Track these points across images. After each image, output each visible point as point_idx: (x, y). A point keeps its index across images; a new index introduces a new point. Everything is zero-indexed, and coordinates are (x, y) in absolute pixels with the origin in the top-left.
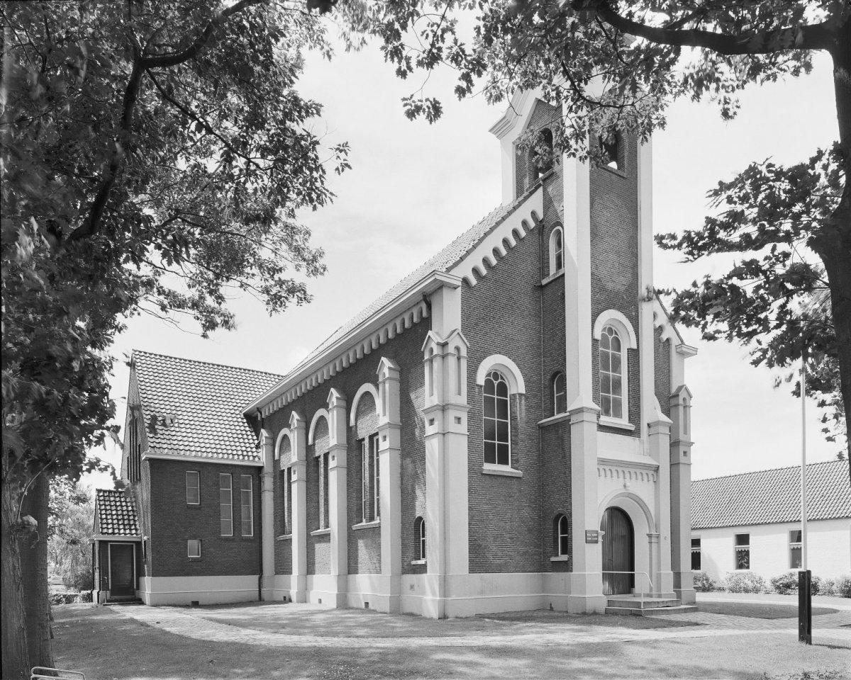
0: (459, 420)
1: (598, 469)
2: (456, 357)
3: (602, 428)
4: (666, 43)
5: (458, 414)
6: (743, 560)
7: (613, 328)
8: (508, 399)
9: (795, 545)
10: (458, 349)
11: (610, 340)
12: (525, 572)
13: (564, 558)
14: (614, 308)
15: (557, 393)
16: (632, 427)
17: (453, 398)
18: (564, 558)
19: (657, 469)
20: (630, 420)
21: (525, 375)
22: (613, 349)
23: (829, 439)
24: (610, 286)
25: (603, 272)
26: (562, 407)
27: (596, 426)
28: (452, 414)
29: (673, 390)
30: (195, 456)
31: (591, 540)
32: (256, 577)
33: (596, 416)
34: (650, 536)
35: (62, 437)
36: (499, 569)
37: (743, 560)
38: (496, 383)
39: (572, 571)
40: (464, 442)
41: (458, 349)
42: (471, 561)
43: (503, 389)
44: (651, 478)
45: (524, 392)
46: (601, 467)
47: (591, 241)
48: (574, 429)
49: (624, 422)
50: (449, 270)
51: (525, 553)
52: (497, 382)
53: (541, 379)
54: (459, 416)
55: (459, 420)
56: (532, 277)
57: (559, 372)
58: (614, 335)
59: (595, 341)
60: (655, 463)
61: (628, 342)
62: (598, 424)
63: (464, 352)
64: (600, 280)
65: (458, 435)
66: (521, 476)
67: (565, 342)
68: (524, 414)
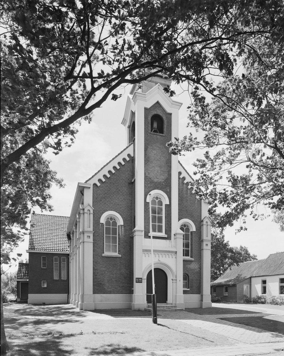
5: (89, 235)
6: (264, 290)
7: (159, 197)
8: (117, 227)
9: (264, 285)
12: (123, 294)
14: (157, 189)
16: (166, 236)
17: (86, 229)
19: (176, 253)
20: (166, 233)
22: (159, 205)
25: (152, 175)
28: (86, 235)
29: (202, 218)
30: (48, 251)
31: (139, 280)
32: (67, 294)
36: (110, 293)
37: (264, 290)
40: (91, 245)
43: (115, 223)
45: (123, 224)
49: (163, 234)
50: (86, 182)
51: (123, 287)
56: (128, 179)
60: (175, 250)
61: (166, 201)
63: (92, 212)
68: (123, 233)
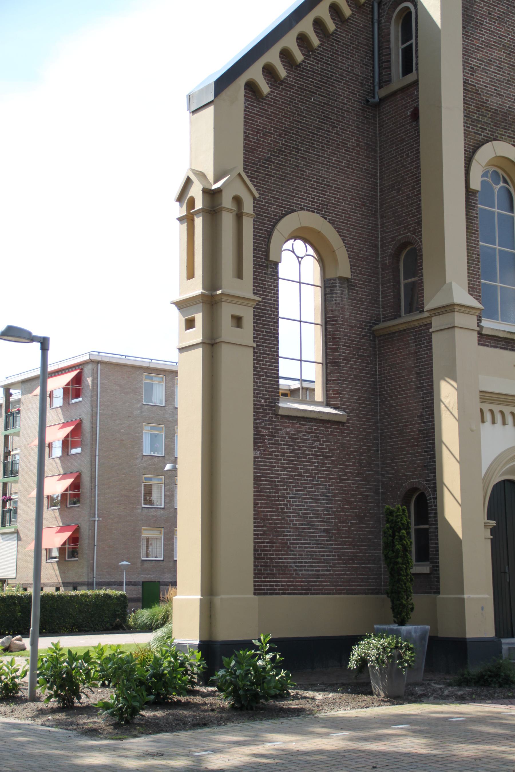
0: (238, 321)
1: (482, 411)
2: (235, 213)
5: (239, 311)
10: (238, 200)
11: (496, 191)
13: (424, 569)
15: (405, 279)
18: (424, 569)
24: (494, 102)
27: (476, 335)
33: (475, 318)
35: (152, 697)
39: (437, 592)
41: (238, 200)
42: (257, 574)
45: (348, 275)
46: (486, 407)
47: (464, 28)
48: (437, 340)
52: (499, 186)
53: (377, 254)
54: (238, 313)
55: (238, 321)
56: (362, 85)
59: (470, 193)
62: (480, 334)
63: (248, 207)
64: (477, 92)
65: (451, 415)
66: (344, 420)
67: (419, 193)
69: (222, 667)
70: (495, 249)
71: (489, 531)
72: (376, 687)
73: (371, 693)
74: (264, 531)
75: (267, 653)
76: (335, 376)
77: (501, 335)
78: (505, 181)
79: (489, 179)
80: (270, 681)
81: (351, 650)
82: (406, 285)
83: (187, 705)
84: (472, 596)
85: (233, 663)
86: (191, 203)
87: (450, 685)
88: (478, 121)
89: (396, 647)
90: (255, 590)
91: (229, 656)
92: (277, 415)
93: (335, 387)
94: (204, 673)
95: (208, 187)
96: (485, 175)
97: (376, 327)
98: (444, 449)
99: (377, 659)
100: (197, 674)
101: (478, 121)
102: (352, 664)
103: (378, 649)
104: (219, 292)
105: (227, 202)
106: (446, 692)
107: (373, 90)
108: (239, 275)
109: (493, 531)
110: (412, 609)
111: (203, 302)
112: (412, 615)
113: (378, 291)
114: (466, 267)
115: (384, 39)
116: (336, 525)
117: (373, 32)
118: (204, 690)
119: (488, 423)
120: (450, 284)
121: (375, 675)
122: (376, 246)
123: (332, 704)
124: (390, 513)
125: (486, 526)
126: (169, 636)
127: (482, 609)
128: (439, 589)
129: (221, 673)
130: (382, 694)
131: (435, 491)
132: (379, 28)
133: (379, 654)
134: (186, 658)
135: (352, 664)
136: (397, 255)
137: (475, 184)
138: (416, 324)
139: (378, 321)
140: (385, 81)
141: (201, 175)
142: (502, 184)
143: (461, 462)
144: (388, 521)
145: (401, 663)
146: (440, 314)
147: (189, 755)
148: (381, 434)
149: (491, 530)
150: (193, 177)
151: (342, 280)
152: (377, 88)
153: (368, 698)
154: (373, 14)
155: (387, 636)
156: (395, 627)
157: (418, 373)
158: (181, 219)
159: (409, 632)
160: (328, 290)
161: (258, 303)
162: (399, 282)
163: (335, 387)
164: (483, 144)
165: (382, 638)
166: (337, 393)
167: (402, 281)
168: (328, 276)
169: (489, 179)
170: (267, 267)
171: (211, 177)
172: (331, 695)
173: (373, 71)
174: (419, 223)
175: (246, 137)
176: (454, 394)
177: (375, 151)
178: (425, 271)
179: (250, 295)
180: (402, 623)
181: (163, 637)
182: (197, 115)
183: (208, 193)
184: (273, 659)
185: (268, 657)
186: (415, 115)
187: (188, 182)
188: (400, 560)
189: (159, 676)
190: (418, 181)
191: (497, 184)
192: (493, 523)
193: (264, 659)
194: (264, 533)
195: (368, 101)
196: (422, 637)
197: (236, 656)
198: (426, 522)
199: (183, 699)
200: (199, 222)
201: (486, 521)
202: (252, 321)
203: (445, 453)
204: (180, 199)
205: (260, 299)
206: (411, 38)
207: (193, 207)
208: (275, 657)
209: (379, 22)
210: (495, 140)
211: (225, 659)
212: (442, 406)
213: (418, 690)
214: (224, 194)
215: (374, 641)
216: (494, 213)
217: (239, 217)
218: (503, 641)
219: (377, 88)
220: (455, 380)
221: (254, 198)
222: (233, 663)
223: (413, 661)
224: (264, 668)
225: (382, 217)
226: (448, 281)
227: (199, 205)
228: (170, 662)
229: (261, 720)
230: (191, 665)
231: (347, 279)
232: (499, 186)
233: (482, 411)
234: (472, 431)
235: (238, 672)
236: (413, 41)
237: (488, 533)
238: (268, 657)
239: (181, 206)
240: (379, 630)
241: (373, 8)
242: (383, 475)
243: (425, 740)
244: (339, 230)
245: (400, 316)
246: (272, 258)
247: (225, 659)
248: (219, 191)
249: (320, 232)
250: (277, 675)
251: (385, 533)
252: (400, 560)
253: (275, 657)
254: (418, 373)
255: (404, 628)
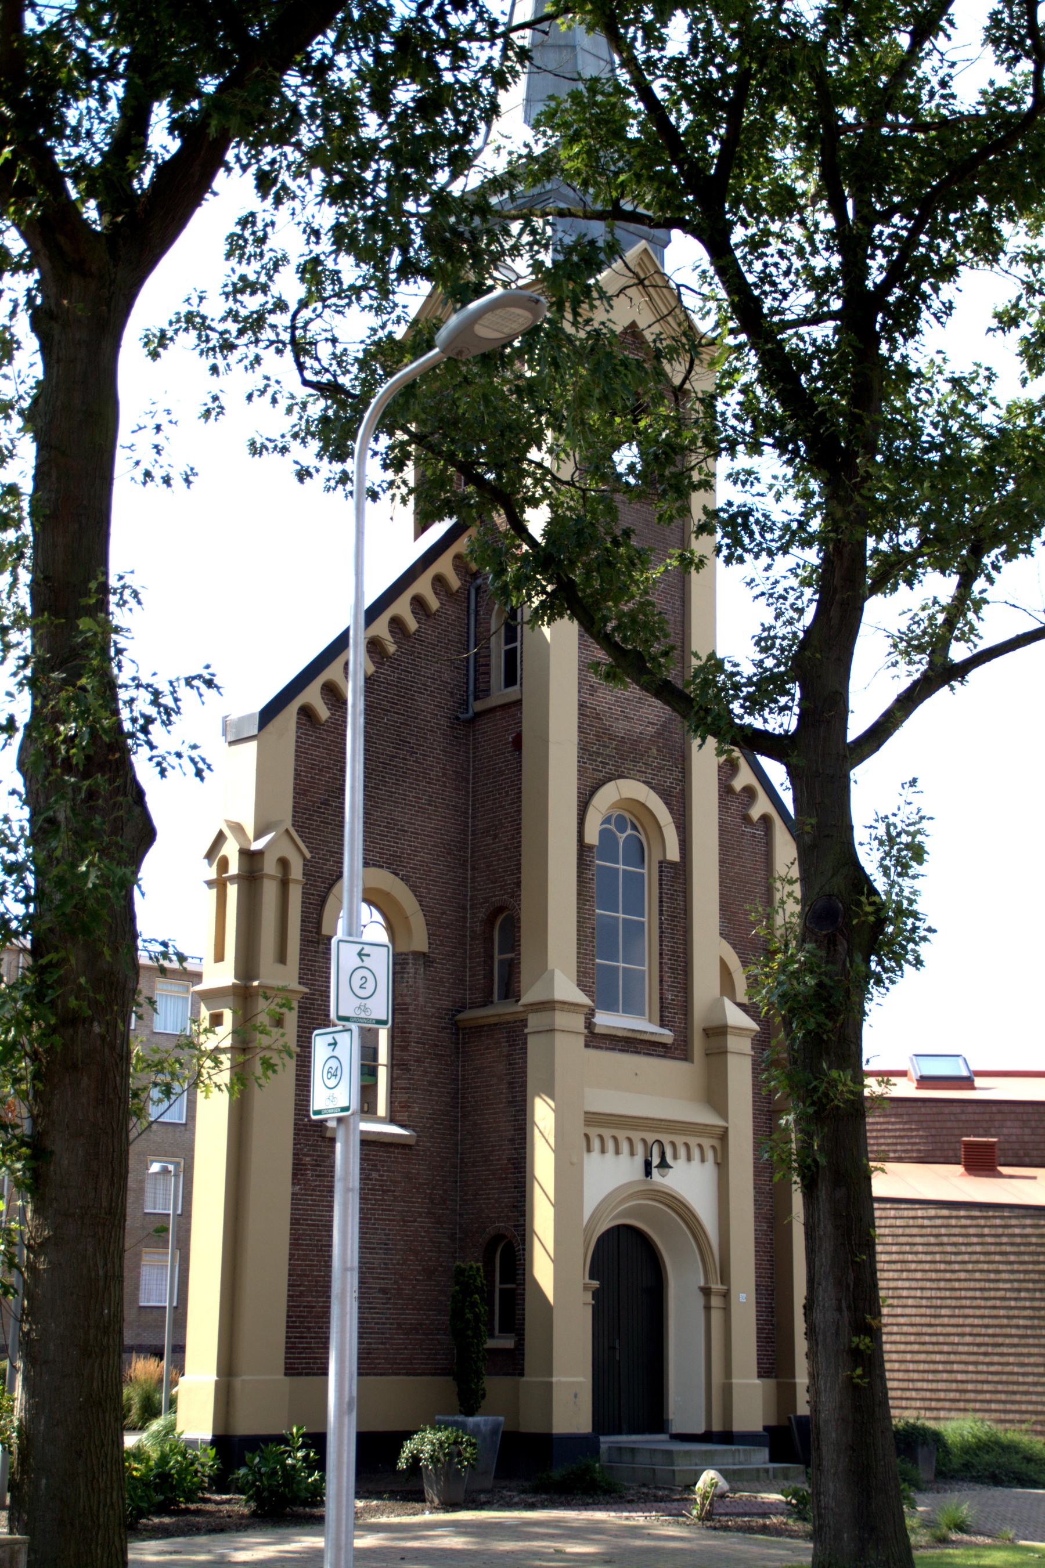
1: (587, 1136)
3: (596, 1039)
4: (731, 99)
10: (284, 863)
13: (507, 1343)
16: (666, 1035)
21: (426, 910)
23: (169, 412)
24: (620, 728)
26: (510, 990)
34: (706, 1292)
38: (622, 837)
39: (522, 1374)
41: (284, 863)
42: (291, 1348)
44: (710, 1155)
46: (593, 1132)
48: (532, 1043)
49: (644, 1025)
52: (624, 835)
53: (465, 918)
57: (500, 910)
58: (629, 832)
59: (583, 848)
63: (297, 871)
66: (412, 1142)
69: (245, 1464)
70: (617, 918)
71: (590, 1295)
72: (430, 1493)
73: (424, 1501)
74: (301, 1292)
75: (299, 1449)
76: (402, 1083)
77: (620, 1034)
78: (634, 827)
79: (612, 827)
80: (300, 1482)
81: (402, 1446)
82: (501, 962)
83: (198, 1512)
84: (563, 1379)
85: (257, 1460)
86: (224, 864)
87: (524, 1492)
88: (598, 754)
89: (455, 1443)
90: (286, 1369)
91: (253, 1452)
92: (324, 1138)
93: (403, 1097)
94: (216, 1475)
95: (245, 847)
96: (607, 820)
97: (460, 1017)
98: (536, 1186)
99: (431, 1457)
100: (209, 1476)
101: (598, 754)
102: (402, 1465)
103: (433, 1444)
104: (256, 983)
105: (270, 867)
106: (516, 1499)
107: (467, 701)
108: (282, 958)
109: (596, 1295)
110: (483, 1396)
111: (234, 994)
112: (483, 1403)
113: (465, 967)
114: (575, 946)
115: (482, 639)
116: (396, 1282)
117: (468, 624)
118: (217, 1497)
119: (596, 1153)
120: (553, 971)
121: (429, 1476)
122: (464, 908)
123: (376, 1511)
124: (461, 1272)
125: (586, 1288)
126: (171, 1428)
127: (576, 1396)
128: (523, 1369)
129: (242, 1471)
130: (436, 1501)
131: (524, 1241)
132: (476, 620)
133: (434, 1451)
134: (196, 1456)
135: (402, 1465)
136: (490, 921)
137: (592, 837)
138: (510, 1018)
139: (462, 1008)
140: (481, 692)
141: (238, 829)
142: (629, 832)
143: (557, 1205)
144: (457, 1283)
145: (460, 1462)
146: (537, 1011)
147: (209, 1552)
148: (462, 1159)
149: (594, 1293)
150: (227, 832)
151: (417, 955)
152: (471, 698)
153: (418, 1506)
154: (469, 603)
155: (446, 1429)
156: (461, 1418)
157: (510, 1083)
158: (210, 884)
159: (477, 1425)
160: (398, 967)
161: (305, 996)
162: (492, 958)
163: (403, 1097)
164: (604, 784)
165: (440, 1430)
166: (406, 1106)
167: (497, 957)
168: (399, 950)
169: (612, 827)
170: (318, 943)
171: (250, 832)
172: (375, 1502)
173: (467, 675)
174: (518, 884)
175: (297, 775)
176: (551, 1116)
177: (467, 781)
178: (523, 949)
179: (294, 985)
180: (470, 1413)
181: (159, 1432)
182: (235, 748)
183: (249, 857)
184: (306, 1458)
185: (300, 1454)
186: (517, 743)
187: (220, 838)
188: (470, 1333)
189: (164, 1477)
190: (518, 830)
191: (623, 831)
192: (596, 1284)
193: (295, 1458)
194: (302, 1294)
195: (458, 718)
196: (494, 1432)
197: (262, 1451)
198: (513, 1281)
199: (193, 1507)
200: (232, 890)
201: (587, 1280)
202: (300, 900)
203: (538, 1192)
204: (210, 855)
205: (307, 990)
206: (515, 640)
207: (226, 871)
208: (308, 1454)
209: (477, 613)
210: (620, 777)
211: (248, 1456)
212: (536, 1131)
213: (483, 1498)
214: (266, 856)
215: (429, 1435)
216: (617, 870)
217: (285, 884)
218: (602, 1439)
219: (471, 698)
220: (553, 1098)
221: (305, 858)
222: (257, 1460)
223: (475, 1460)
224: (293, 1466)
225: (473, 869)
226: (550, 967)
227: (234, 869)
228: (177, 1462)
229: (288, 1526)
230: (203, 1465)
231: (424, 954)
232: (624, 835)
233: (587, 1136)
234: (572, 1164)
235: (263, 1470)
236: (518, 644)
237: (589, 1297)
238: (300, 1454)
239: (210, 865)
240: (440, 1423)
241: (469, 594)
242: (461, 1215)
243: (463, 1539)
244: (414, 888)
245: (492, 1002)
246: (325, 931)
247: (248, 1456)
248: (260, 853)
249: (388, 894)
250: (310, 1475)
251: (453, 1297)
252: (470, 1333)
253: (308, 1454)
254: (510, 1083)
255: (471, 1420)
